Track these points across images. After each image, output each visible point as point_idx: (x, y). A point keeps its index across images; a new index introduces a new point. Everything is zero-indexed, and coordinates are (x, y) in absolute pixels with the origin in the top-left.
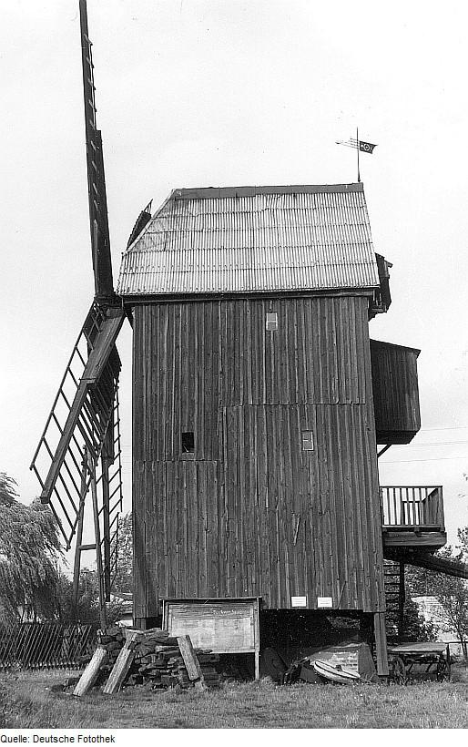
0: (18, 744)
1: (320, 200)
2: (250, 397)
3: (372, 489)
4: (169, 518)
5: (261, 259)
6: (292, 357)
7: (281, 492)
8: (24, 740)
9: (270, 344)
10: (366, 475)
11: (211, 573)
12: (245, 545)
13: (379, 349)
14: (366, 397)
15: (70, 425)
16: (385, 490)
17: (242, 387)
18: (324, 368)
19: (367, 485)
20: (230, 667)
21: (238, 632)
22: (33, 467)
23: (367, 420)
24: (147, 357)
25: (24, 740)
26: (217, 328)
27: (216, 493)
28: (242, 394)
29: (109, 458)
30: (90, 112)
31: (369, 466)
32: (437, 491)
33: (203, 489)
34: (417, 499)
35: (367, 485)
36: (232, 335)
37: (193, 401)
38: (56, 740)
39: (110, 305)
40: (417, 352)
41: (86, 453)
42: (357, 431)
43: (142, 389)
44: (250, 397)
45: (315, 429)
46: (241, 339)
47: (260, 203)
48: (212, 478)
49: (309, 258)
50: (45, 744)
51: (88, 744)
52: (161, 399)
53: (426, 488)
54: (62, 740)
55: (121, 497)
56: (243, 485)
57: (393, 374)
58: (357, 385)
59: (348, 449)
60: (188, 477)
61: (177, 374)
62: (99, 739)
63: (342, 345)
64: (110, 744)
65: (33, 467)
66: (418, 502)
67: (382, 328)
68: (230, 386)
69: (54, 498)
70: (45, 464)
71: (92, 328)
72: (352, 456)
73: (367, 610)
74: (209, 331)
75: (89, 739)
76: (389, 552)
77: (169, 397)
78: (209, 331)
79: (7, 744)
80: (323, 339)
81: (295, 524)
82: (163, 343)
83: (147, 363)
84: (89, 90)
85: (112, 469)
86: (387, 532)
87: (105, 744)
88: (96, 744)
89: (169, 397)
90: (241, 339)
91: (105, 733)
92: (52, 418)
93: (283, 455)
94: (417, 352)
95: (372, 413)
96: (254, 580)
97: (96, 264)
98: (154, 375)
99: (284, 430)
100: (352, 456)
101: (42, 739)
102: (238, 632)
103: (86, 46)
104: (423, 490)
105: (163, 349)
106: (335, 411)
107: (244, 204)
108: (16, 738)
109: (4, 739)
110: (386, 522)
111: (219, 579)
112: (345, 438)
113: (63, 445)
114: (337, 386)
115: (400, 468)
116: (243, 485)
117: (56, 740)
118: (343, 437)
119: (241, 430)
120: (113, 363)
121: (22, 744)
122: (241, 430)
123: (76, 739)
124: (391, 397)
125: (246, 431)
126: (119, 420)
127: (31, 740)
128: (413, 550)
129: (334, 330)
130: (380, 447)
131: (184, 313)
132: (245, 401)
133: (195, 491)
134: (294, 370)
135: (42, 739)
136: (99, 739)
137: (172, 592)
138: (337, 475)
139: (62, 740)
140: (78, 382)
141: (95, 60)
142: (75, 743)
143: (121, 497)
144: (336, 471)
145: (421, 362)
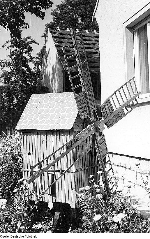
8: (8, 237)
25: (8, 237)
54: (20, 237)
62: (32, 236)
75: (28, 236)
101: (13, 237)
108: (5, 236)
109: (1, 236)
121: (7, 238)
127: (10, 237)
136: (32, 236)
139: (20, 237)
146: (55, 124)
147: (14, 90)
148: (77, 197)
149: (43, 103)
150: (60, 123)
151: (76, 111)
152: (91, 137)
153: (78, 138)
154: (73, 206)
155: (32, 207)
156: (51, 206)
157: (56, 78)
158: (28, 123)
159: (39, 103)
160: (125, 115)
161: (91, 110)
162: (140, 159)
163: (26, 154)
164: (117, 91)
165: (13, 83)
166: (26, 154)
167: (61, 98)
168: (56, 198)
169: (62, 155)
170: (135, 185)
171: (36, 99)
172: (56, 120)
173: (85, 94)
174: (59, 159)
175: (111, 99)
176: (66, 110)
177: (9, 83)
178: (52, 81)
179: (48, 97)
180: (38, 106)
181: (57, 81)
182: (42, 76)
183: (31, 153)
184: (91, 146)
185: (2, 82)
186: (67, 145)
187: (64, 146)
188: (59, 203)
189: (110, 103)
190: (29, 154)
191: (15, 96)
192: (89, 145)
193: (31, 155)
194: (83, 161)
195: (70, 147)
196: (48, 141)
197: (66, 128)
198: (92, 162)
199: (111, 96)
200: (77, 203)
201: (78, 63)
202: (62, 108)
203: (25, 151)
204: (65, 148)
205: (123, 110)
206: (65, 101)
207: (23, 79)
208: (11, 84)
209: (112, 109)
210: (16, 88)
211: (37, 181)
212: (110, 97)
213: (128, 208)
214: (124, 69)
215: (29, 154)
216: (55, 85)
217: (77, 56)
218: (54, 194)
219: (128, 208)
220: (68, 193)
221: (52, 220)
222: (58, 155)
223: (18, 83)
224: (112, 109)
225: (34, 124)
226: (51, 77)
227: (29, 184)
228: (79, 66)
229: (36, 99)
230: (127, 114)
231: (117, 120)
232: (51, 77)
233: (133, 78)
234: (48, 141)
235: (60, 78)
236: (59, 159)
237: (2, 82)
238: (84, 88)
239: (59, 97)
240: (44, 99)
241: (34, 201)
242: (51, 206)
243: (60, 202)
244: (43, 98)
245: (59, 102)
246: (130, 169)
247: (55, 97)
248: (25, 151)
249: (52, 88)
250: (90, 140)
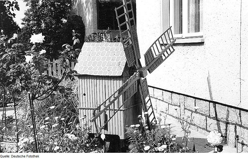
8: (8, 156)
25: (8, 156)
54: (21, 157)
62: (34, 156)
75: (30, 156)
101: (14, 156)
108: (5, 156)
109: (1, 156)
121: (7, 158)
127: (10, 156)
136: (34, 156)
139: (21, 157)
146: (107, 71)
147: (42, 14)
148: (125, 131)
149: (95, 51)
150: (111, 70)
151: (125, 61)
152: (137, 82)
153: (127, 84)
154: (122, 137)
155: (93, 140)
156: (103, 137)
157: (90, 6)
158: (83, 69)
159: (91, 51)
160: (163, 60)
161: (137, 59)
162: (172, 92)
163: (81, 95)
164: (157, 41)
165: (40, 7)
166: (81, 95)
167: (111, 47)
168: (107, 130)
169: (115, 99)
170: (167, 115)
171: (88, 47)
172: (108, 67)
173: (132, 46)
174: (113, 102)
175: (152, 48)
176: (116, 58)
177: (37, 7)
178: (85, 10)
179: (99, 46)
180: (91, 54)
181: (91, 10)
182: (75, 4)
183: (86, 94)
184: (137, 89)
185: (29, 5)
186: (119, 90)
187: (117, 91)
188: (113, 135)
189: (151, 52)
190: (85, 95)
191: (44, 21)
192: (134, 88)
193: (86, 96)
194: (129, 101)
195: (121, 91)
196: (101, 84)
197: (117, 75)
198: (135, 102)
199: (152, 46)
200: (125, 135)
201: (127, 20)
202: (112, 57)
203: (81, 93)
204: (118, 92)
205: (161, 57)
206: (114, 51)
207: (51, 2)
208: (39, 8)
209: (153, 56)
210: (44, 12)
211: (98, 120)
212: (151, 47)
213: (168, 140)
214: (160, 9)
215: (85, 95)
216: (88, 14)
217: (126, 14)
218: (106, 128)
219: (168, 140)
220: (117, 126)
221: (104, 148)
222: (112, 99)
223: (47, 6)
224: (153, 57)
225: (88, 70)
226: (85, 5)
227: (92, 123)
228: (128, 23)
229: (88, 47)
230: (165, 59)
231: (157, 66)
232: (85, 5)
233: (170, 28)
234: (101, 84)
235: (94, 8)
236: (113, 102)
237: (29, 5)
238: (132, 41)
239: (109, 46)
240: (96, 48)
241: (94, 134)
242: (103, 137)
243: (111, 134)
244: (95, 46)
245: (109, 51)
246: (163, 101)
247: (105, 47)
248: (81, 93)
249: (85, 17)
250: (135, 84)
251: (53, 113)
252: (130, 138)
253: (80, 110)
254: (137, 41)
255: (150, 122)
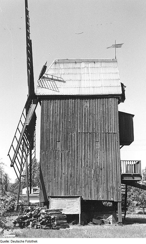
0: (6, 243)
1: (103, 64)
2: (79, 130)
3: (118, 161)
4: (52, 169)
5: (83, 84)
6: (93, 117)
7: (88, 162)
8: (8, 242)
9: (86, 112)
10: (116, 156)
11: (65, 187)
12: (76, 179)
13: (121, 114)
14: (117, 131)
15: (21, 140)
16: (122, 161)
17: (76, 126)
18: (103, 121)
19: (116, 160)
20: (72, 219)
21: (73, 207)
22: (8, 155)
23: (117, 138)
24: (45, 116)
25: (8, 242)
26: (68, 107)
27: (67, 162)
28: (76, 129)
29: (32, 147)
30: (28, 34)
31: (117, 154)
32: (139, 162)
33: (63, 160)
34: (130, 164)
35: (116, 160)
36: (73, 109)
37: (60, 131)
38: (18, 242)
39: (33, 98)
40: (133, 116)
41: (23, 144)
42: (114, 142)
43: (44, 126)
44: (79, 130)
45: (100, 141)
46: (76, 111)
47: (83, 65)
48: (66, 156)
49: (99, 84)
50: (15, 243)
51: (29, 243)
52: (50, 130)
53: (136, 161)
54: (20, 242)
55: (35, 150)
56: (76, 159)
57: (126, 123)
58: (114, 126)
59: (110, 148)
60: (58, 156)
61: (55, 122)
62: (32, 241)
63: (109, 113)
64: (36, 243)
65: (8, 155)
66: (131, 165)
67: (123, 108)
68: (72, 126)
69: (15, 165)
70: (12, 154)
71: (27, 107)
72: (111, 150)
73: (115, 201)
74: (66, 108)
75: (29, 241)
76: (123, 182)
77: (53, 129)
78: (66, 108)
79: (2, 243)
80: (103, 111)
81: (93, 172)
82: (51, 111)
83: (45, 118)
84: (27, 20)
85: (33, 151)
86: (123, 176)
87: (34, 243)
88: (31, 243)
89: (53, 129)
90: (76, 111)
91: (34, 239)
92: (15, 137)
93: (89, 149)
94: (133, 116)
95: (118, 136)
96: (79, 190)
97: (29, 77)
98: (48, 122)
99: (90, 141)
100: (111, 150)
101: (14, 241)
102: (73, 207)
103: (27, 12)
104: (135, 162)
105: (51, 113)
106: (107, 135)
107: (78, 65)
108: (5, 241)
109: (1, 241)
110: (122, 172)
111: (67, 190)
112: (109, 144)
113: (18, 147)
114: (107, 127)
115: (127, 154)
116: (76, 159)
117: (18, 242)
118: (109, 144)
119: (76, 141)
120: (34, 117)
121: (7, 243)
122: (76, 141)
123: (25, 242)
124: (126, 131)
125: (77, 141)
126: (35, 140)
127: (10, 242)
128: (130, 180)
129: (107, 108)
130: (121, 146)
131: (58, 102)
132: (77, 131)
133: (60, 161)
134: (93, 121)
135: (14, 241)
136: (32, 241)
137: (52, 194)
138: (107, 156)
139: (20, 242)
140: (23, 125)
141: (31, 24)
142: (25, 243)
143: (35, 150)
144: (106, 155)
145: (134, 119)
251: (28, 223)
252: (68, 157)
253: (119, 203)
254: (57, 95)
255: (32, 159)
